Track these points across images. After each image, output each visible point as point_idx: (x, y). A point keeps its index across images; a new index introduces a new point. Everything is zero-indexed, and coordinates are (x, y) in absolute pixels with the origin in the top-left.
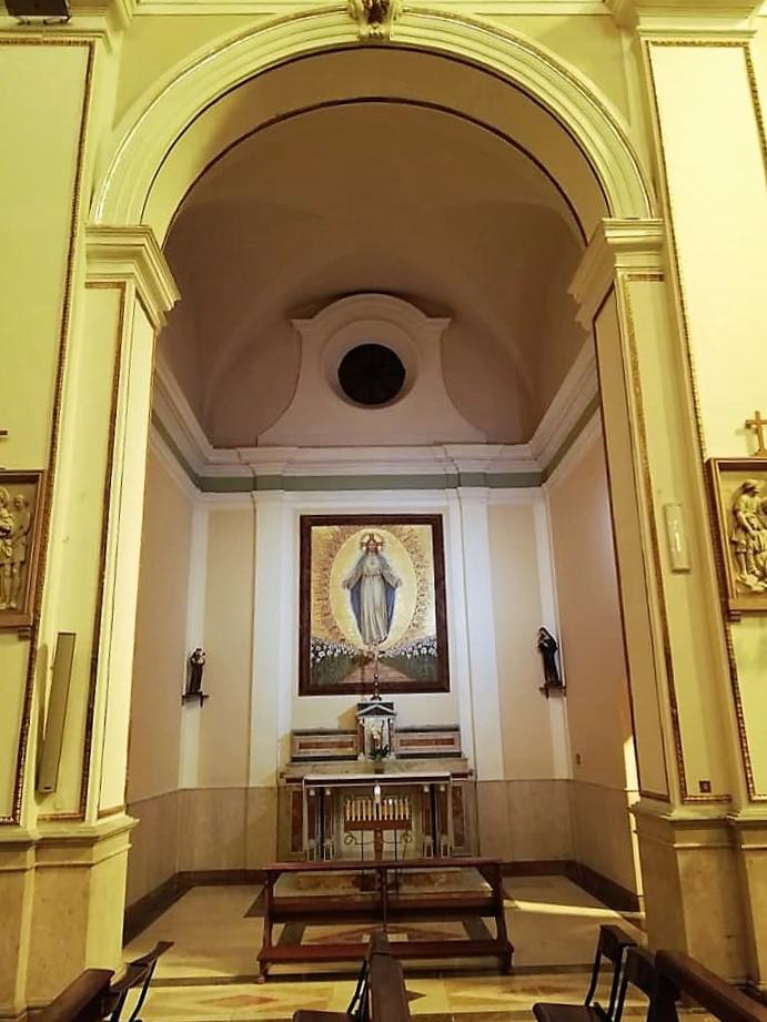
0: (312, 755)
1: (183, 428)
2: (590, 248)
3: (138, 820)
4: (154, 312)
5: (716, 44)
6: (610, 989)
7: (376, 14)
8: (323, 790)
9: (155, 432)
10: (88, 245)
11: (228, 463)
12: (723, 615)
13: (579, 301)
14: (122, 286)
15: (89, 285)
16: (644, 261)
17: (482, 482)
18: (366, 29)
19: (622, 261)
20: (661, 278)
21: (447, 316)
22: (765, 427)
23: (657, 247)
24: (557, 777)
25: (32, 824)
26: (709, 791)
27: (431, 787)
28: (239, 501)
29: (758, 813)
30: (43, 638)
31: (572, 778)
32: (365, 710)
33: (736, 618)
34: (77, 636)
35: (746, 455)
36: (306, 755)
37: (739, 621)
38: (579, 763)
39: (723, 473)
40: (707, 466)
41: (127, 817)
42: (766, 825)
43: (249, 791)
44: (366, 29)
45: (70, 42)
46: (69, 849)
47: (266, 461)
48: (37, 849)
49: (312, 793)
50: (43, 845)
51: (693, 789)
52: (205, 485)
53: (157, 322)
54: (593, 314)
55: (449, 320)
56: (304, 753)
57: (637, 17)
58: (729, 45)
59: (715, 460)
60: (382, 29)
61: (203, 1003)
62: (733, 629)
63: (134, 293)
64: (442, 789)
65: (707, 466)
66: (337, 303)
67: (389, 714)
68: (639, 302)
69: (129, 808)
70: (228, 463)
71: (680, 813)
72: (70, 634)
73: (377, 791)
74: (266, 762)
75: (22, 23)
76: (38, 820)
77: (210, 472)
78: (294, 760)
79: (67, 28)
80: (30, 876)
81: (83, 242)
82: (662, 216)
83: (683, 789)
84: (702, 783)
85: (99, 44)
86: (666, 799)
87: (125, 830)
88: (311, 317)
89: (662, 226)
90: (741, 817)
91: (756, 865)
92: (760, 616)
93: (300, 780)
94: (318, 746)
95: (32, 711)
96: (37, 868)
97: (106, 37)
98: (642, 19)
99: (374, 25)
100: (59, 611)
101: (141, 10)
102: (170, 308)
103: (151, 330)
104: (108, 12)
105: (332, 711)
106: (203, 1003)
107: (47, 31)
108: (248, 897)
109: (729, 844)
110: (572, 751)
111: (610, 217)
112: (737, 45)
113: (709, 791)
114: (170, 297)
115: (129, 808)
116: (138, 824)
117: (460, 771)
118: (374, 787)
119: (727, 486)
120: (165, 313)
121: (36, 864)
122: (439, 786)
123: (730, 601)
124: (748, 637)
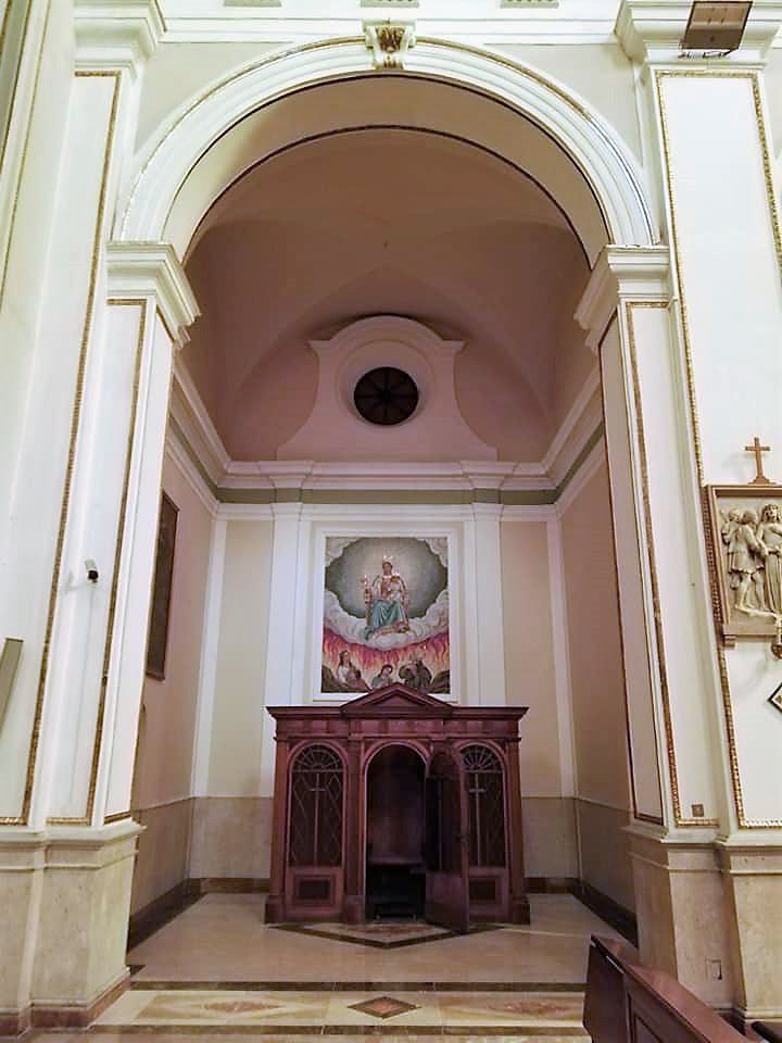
2: (594, 273)
3: (145, 827)
4: (174, 327)
7: (391, 40)
10: (109, 261)
12: (717, 640)
13: (585, 327)
14: (142, 302)
15: (111, 302)
16: (654, 288)
18: (381, 57)
19: (625, 287)
20: (664, 305)
21: (460, 340)
23: (663, 276)
26: (702, 815)
28: (261, 511)
33: (731, 643)
37: (733, 646)
39: (720, 500)
40: (705, 492)
41: (134, 823)
44: (381, 57)
45: (729, 75)
47: (286, 473)
48: (46, 851)
50: (53, 847)
51: (686, 814)
52: (223, 495)
53: (176, 336)
54: (598, 341)
55: (461, 344)
57: (645, 50)
60: (397, 57)
62: (727, 653)
63: (155, 308)
65: (705, 492)
66: (351, 327)
68: (643, 331)
69: (136, 813)
70: (243, 474)
71: (673, 835)
76: (48, 822)
80: (38, 877)
82: (666, 243)
85: (125, 73)
86: (660, 822)
87: (133, 834)
89: (667, 252)
90: (730, 842)
92: (765, 641)
96: (46, 868)
97: (133, 66)
98: (649, 51)
101: (167, 37)
103: (171, 344)
104: (135, 42)
107: (712, 64)
109: (716, 869)
112: (112, 74)
114: (190, 311)
115: (136, 813)
116: (145, 830)
119: (721, 507)
120: (188, 328)
121: (45, 865)
123: (724, 626)
124: (744, 662)
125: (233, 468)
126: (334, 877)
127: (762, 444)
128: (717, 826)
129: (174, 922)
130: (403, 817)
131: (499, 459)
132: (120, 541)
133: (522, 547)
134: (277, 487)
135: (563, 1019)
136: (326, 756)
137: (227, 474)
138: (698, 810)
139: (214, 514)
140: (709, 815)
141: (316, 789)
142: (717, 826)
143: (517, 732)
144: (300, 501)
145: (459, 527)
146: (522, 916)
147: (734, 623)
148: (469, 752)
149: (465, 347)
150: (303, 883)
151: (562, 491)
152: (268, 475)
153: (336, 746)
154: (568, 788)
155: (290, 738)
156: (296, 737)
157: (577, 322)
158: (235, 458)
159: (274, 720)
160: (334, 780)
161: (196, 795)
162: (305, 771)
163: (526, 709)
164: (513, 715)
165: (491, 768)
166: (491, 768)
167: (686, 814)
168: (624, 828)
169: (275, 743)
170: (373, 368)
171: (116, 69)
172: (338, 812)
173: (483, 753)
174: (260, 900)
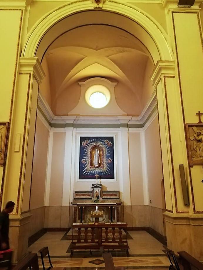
0: (106, 198)
1: (46, 110)
8: (82, 207)
18: (96, 5)
24: (145, 205)
27: (111, 207)
32: (95, 186)
35: (196, 123)
36: (107, 198)
38: (151, 202)
43: (132, 206)
44: (96, 5)
49: (79, 208)
52: (52, 125)
56: (77, 197)
59: (187, 124)
60: (101, 5)
64: (114, 208)
67: (100, 187)
72: (182, 165)
73: (97, 208)
74: (67, 199)
75: (184, 7)
77: (52, 122)
78: (75, 199)
79: (191, 9)
86: (172, 212)
93: (76, 204)
94: (84, 195)
99: (98, 3)
105: (87, 184)
108: (61, 235)
110: (149, 199)
117: (119, 203)
118: (96, 207)
122: (113, 207)
127: (198, 113)
129: (43, 237)
132: (169, 124)
133: (133, 140)
134: (66, 123)
135: (154, 71)
139: (49, 130)
144: (76, 127)
145: (117, 134)
147: (23, 8)
149: (117, 84)
158: (56, 115)
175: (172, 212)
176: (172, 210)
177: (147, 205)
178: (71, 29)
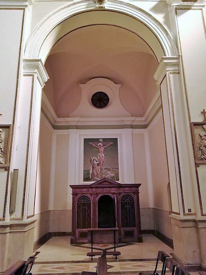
5: (15, 9)
6: (163, 265)
9: (43, 116)
11: (62, 121)
13: (156, 79)
14: (33, 75)
15: (25, 75)
17: (85, 178)
21: (120, 84)
22: (205, 113)
23: (178, 65)
24: (150, 207)
25: (8, 221)
29: (204, 218)
30: (11, 170)
31: (154, 208)
34: (19, 170)
35: (201, 121)
37: (199, 166)
39: (195, 126)
42: (205, 221)
46: (19, 227)
47: (72, 121)
50: (11, 226)
51: (187, 212)
52: (55, 127)
55: (121, 85)
58: (19, 9)
59: (192, 123)
61: (52, 268)
63: (36, 77)
70: (62, 121)
81: (22, 64)
83: (184, 211)
84: (189, 209)
88: (85, 84)
91: (203, 232)
95: (8, 191)
100: (16, 162)
102: (46, 81)
106: (52, 268)
111: (165, 56)
112: (22, 9)
113: (191, 211)
114: (46, 78)
125: (58, 120)
126: (134, 230)
128: (195, 215)
130: (108, 213)
131: (132, 116)
136: (84, 197)
137: (56, 122)
138: (190, 210)
140: (193, 211)
141: (128, 206)
142: (195, 215)
143: (138, 191)
146: (140, 241)
148: (124, 197)
150: (126, 232)
151: (149, 124)
152: (67, 121)
153: (89, 195)
154: (152, 205)
155: (97, 193)
156: (121, 193)
157: (154, 78)
159: (72, 189)
160: (89, 205)
161: (50, 210)
162: (124, 201)
163: (141, 184)
164: (138, 186)
165: (88, 201)
166: (88, 201)
167: (187, 212)
168: (169, 216)
169: (72, 195)
170: (108, 96)
171: (201, 8)
172: (90, 214)
173: (129, 196)
174: (69, 238)
175: (179, 214)
176: (179, 213)
177: (152, 207)
178: (70, 32)
